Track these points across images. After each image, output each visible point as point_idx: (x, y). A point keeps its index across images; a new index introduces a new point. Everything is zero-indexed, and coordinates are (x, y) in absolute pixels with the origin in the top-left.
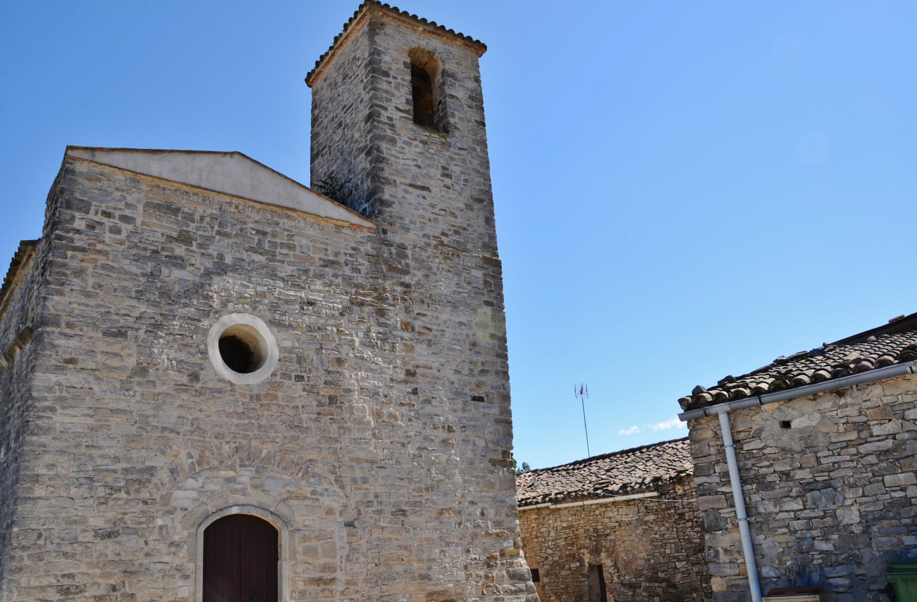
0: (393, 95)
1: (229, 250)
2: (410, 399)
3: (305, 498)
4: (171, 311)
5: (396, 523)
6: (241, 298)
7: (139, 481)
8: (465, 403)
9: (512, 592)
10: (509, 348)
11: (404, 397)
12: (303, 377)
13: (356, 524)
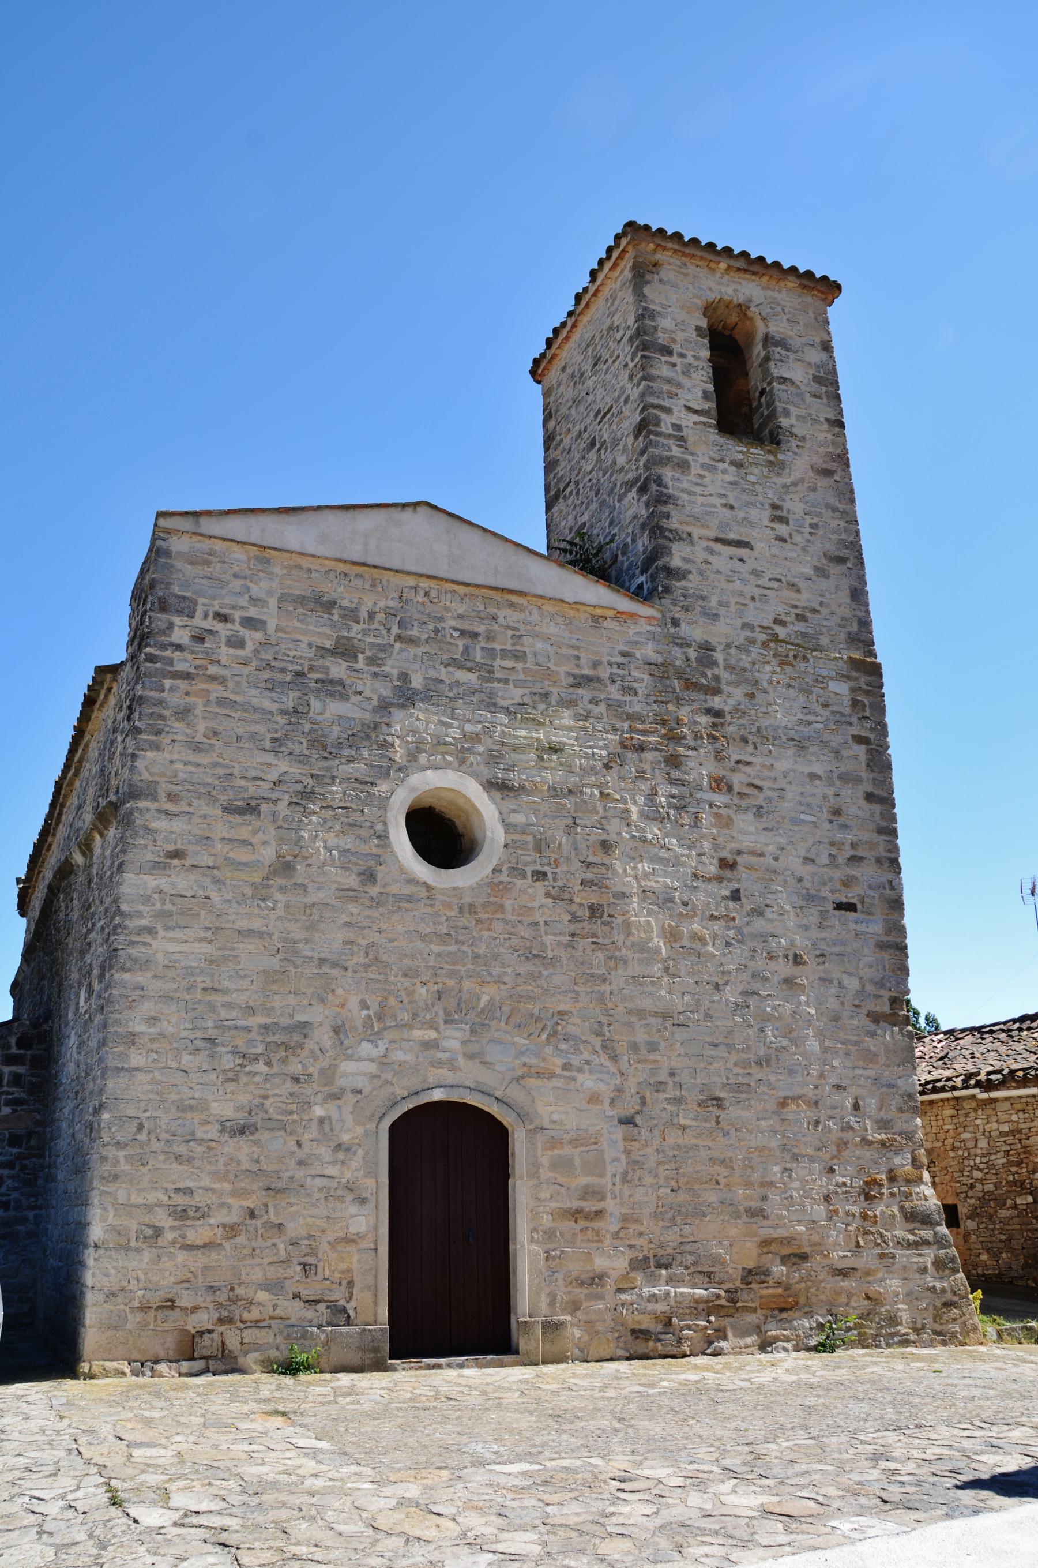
0: (679, 386)
1: (417, 666)
2: (727, 908)
3: (552, 1075)
4: (328, 769)
5: (706, 1121)
6: (439, 744)
7: (287, 1046)
8: (823, 913)
9: (910, 1245)
10: (898, 818)
11: (718, 905)
12: (545, 874)
13: (639, 1120)
